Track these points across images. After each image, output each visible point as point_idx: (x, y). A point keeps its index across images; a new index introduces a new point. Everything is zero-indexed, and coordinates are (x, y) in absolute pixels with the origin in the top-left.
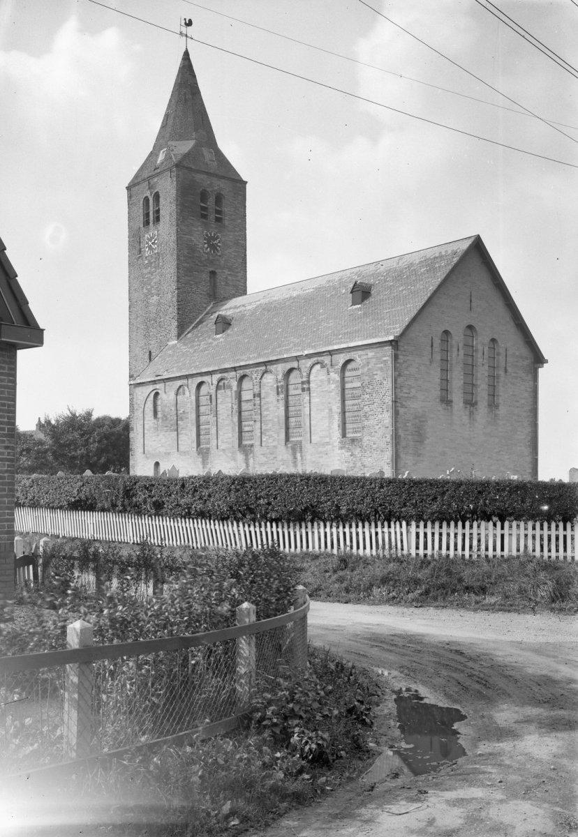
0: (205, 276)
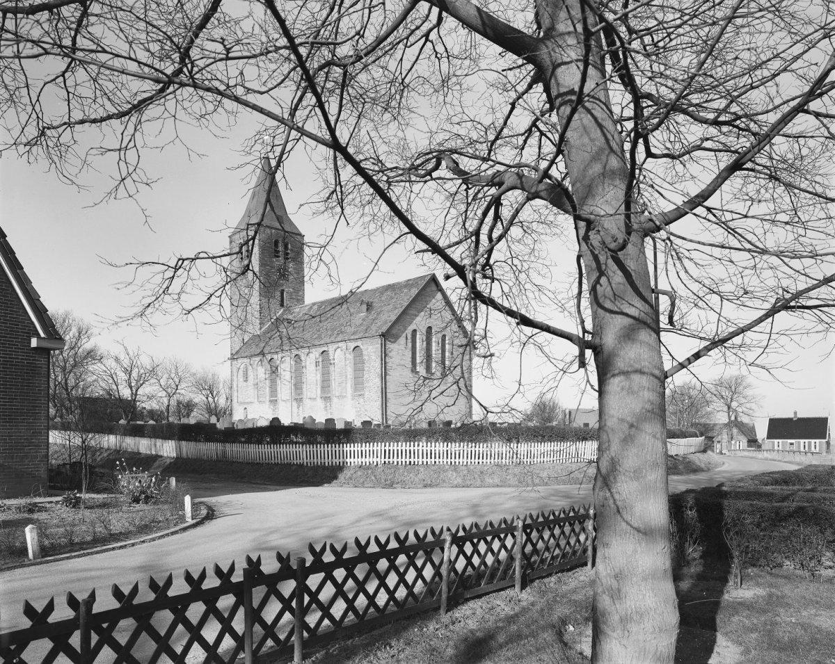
0: (278, 294)
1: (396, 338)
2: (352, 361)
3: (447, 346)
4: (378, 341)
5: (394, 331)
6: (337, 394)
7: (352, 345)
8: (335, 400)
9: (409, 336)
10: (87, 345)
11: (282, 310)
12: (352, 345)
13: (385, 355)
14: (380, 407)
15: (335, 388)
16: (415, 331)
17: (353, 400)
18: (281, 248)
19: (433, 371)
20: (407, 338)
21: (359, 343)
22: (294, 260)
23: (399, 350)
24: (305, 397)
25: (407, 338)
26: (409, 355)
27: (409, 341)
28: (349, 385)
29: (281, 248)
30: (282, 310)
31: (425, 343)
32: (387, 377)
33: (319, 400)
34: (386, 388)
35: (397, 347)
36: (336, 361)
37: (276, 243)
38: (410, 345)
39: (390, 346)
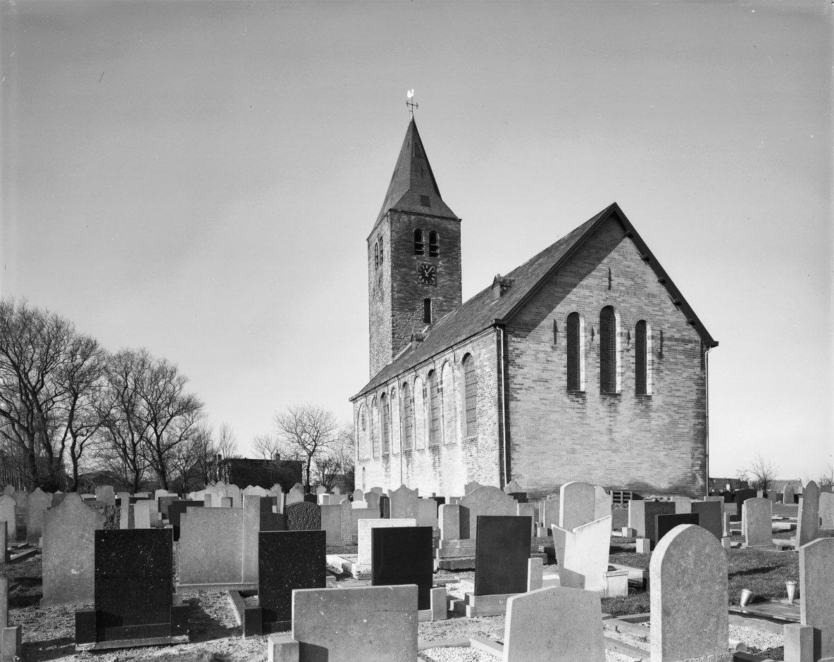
0: (422, 305)
1: (529, 327)
2: (463, 381)
3: (649, 343)
4: (492, 336)
5: (527, 318)
6: (447, 442)
7: (461, 353)
8: (444, 450)
9: (562, 325)
10: (336, 422)
11: (427, 327)
12: (461, 353)
13: (506, 361)
14: (497, 461)
15: (445, 435)
16: (573, 319)
17: (463, 449)
18: (424, 240)
19: (618, 388)
20: (555, 330)
21: (468, 349)
22: (444, 254)
23: (537, 352)
24: (413, 448)
25: (555, 330)
26: (561, 360)
27: (562, 334)
28: (459, 423)
29: (424, 240)
30: (427, 327)
31: (597, 337)
32: (512, 404)
33: (427, 452)
34: (508, 424)
35: (533, 346)
36: (444, 385)
37: (418, 235)
38: (563, 342)
39: (517, 344)
